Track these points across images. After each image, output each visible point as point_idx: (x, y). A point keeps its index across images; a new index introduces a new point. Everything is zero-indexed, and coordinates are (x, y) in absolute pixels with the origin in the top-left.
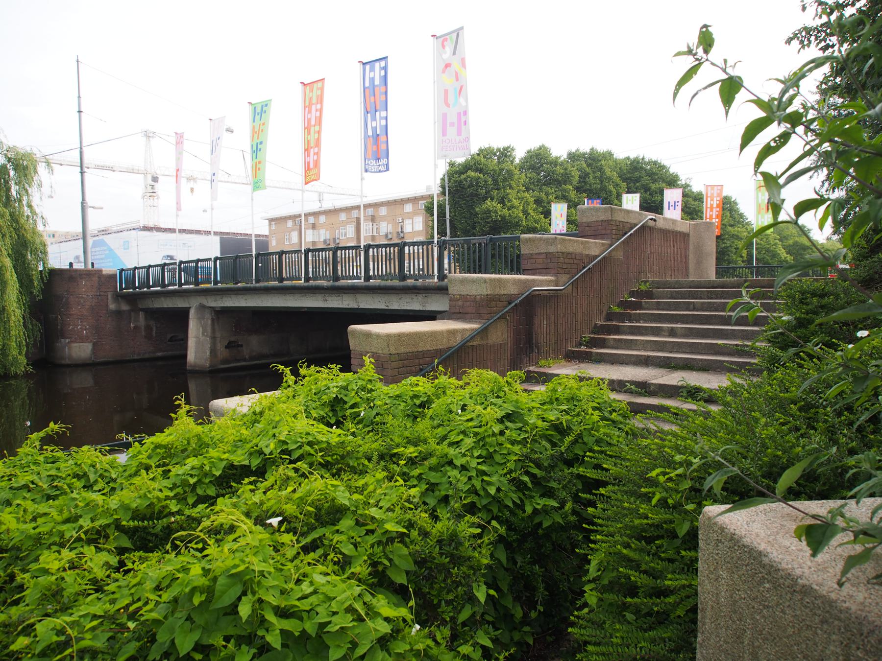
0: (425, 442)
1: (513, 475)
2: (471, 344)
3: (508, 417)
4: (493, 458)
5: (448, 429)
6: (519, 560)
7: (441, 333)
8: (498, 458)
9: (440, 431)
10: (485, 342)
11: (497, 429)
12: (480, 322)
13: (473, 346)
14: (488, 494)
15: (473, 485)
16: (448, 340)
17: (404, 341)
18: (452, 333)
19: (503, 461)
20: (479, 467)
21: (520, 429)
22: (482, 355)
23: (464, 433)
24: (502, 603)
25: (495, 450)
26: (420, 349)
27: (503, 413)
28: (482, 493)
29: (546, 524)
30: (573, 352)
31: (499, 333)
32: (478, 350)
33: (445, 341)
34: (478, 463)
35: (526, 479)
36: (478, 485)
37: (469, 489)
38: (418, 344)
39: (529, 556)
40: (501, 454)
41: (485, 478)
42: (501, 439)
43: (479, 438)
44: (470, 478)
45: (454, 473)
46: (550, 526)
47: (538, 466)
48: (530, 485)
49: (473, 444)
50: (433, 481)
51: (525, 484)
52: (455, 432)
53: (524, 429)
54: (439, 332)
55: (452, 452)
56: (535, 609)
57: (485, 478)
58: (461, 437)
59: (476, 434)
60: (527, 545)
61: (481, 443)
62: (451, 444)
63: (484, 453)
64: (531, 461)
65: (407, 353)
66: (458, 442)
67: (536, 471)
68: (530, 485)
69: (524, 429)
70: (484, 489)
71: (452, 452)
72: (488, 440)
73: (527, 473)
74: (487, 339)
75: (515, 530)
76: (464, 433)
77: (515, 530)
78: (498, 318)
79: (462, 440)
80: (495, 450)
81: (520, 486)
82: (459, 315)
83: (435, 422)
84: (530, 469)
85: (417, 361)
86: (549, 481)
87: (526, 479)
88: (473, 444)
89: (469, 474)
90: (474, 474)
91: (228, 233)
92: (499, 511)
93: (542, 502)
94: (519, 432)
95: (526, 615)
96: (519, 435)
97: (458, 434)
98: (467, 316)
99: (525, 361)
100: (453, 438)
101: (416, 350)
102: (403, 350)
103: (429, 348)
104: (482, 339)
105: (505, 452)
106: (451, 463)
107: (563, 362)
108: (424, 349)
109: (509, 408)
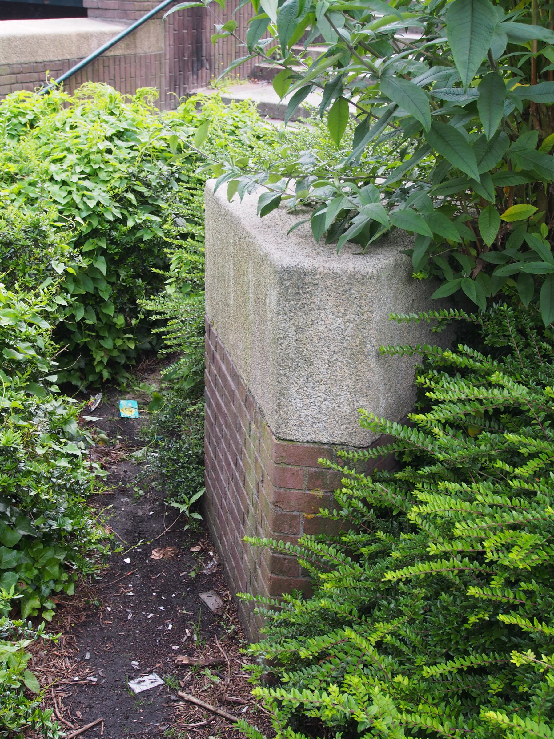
0: (26, 159)
1: (116, 191)
2: (112, 54)
3: (120, 135)
4: (97, 175)
5: (52, 146)
6: (123, 274)
7: (68, 37)
8: (103, 175)
9: (45, 149)
10: (132, 52)
11: (104, 145)
12: (126, 23)
13: (114, 57)
14: (88, 208)
15: (73, 199)
16: (79, 48)
17: (15, 46)
18: (85, 37)
19: (108, 179)
20: (82, 183)
21: (131, 148)
22: (128, 68)
23: (68, 150)
24: (104, 311)
25: (100, 168)
26: (40, 59)
27: (114, 131)
28: (81, 206)
29: (146, 238)
30: (262, 69)
31: (153, 40)
32: (123, 63)
33: (74, 48)
34: (80, 179)
35: (130, 196)
36: (78, 199)
37: (68, 203)
38: (37, 52)
39: (132, 270)
40: (106, 172)
41: (85, 192)
42: (107, 157)
43: (83, 154)
44: (70, 193)
45: (54, 188)
46: (150, 240)
47: (148, 185)
48: (134, 202)
49: (77, 161)
50: (32, 195)
51: (129, 201)
52: (59, 149)
53: (135, 148)
54: (66, 36)
55: (53, 168)
56: (137, 318)
57: (85, 192)
58: (65, 153)
59: (80, 151)
60: (130, 260)
61: (86, 160)
62: (54, 161)
63: (88, 170)
64: (138, 179)
65: (21, 64)
66: (61, 160)
67: (142, 189)
68: (134, 202)
69: (135, 148)
70: (84, 203)
71: (53, 168)
72: (92, 157)
73: (134, 191)
74: (136, 47)
75: (116, 244)
76: (68, 150)
77: (116, 244)
78: (150, 18)
79: (65, 157)
80: (100, 168)
81: (118, 198)
82: (97, 12)
83: (42, 141)
84: (136, 188)
85: (36, 75)
86: (156, 200)
87: (130, 196)
88: (77, 161)
89: (69, 189)
90: (74, 189)
91: (236, 377)
92: (100, 223)
93: (144, 216)
94: (129, 150)
95: (128, 324)
96: (129, 154)
97: (62, 151)
98: (110, 13)
99: (190, 80)
100: (57, 155)
101: (33, 60)
102: (15, 59)
103: (52, 58)
104: (128, 47)
105: (111, 169)
106: (52, 179)
107: (247, 83)
108: (45, 59)
109: (122, 126)
